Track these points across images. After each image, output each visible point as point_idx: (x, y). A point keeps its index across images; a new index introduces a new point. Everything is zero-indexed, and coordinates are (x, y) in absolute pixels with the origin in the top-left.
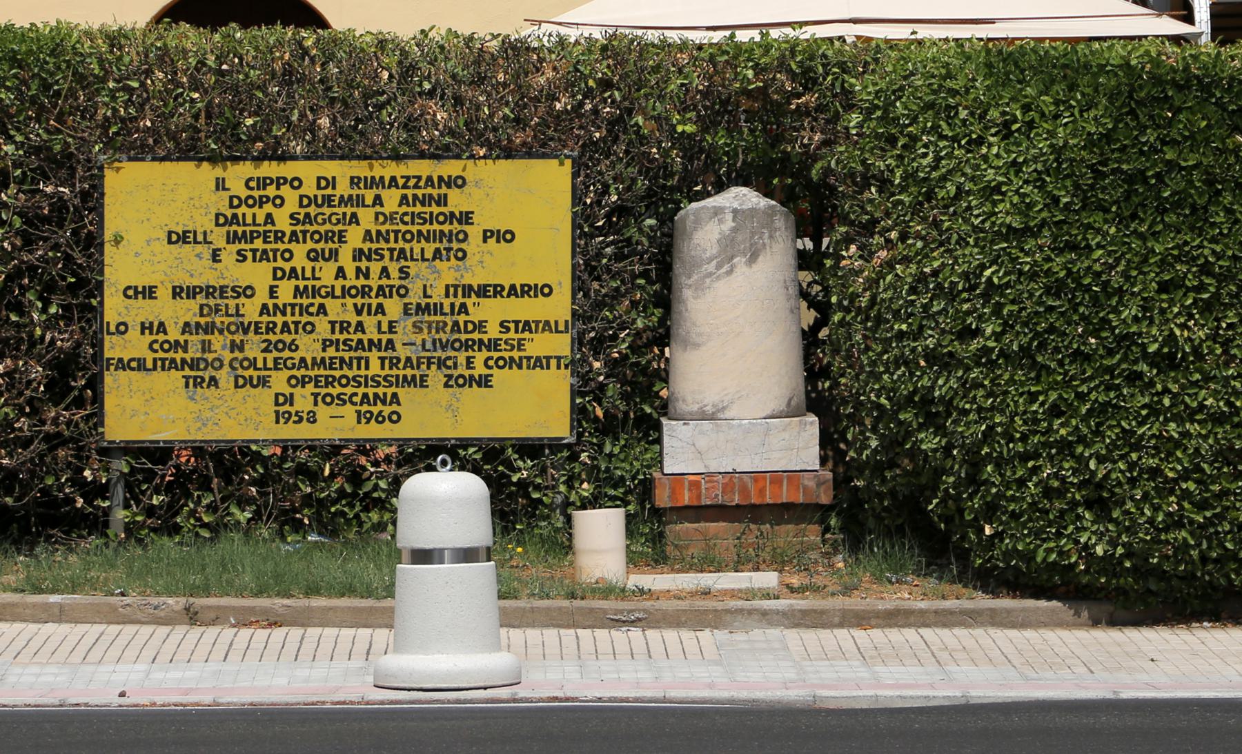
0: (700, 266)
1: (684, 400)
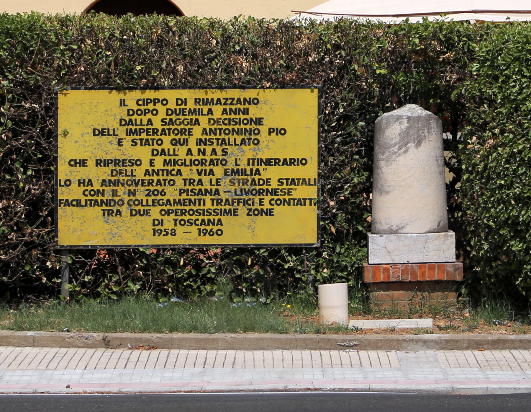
0: (389, 148)
1: (380, 223)
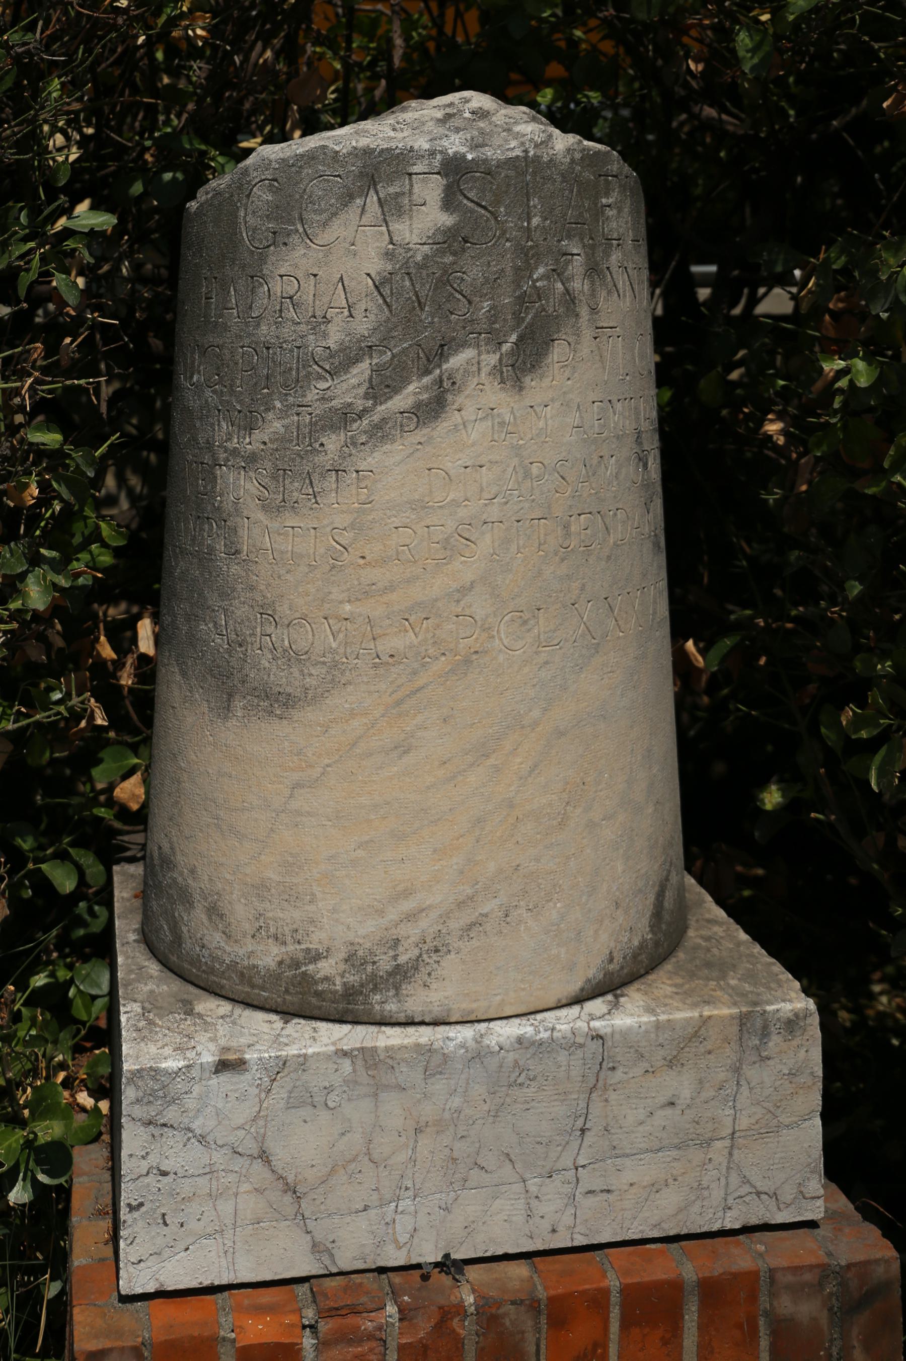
0: (301, 383)
1: (214, 912)
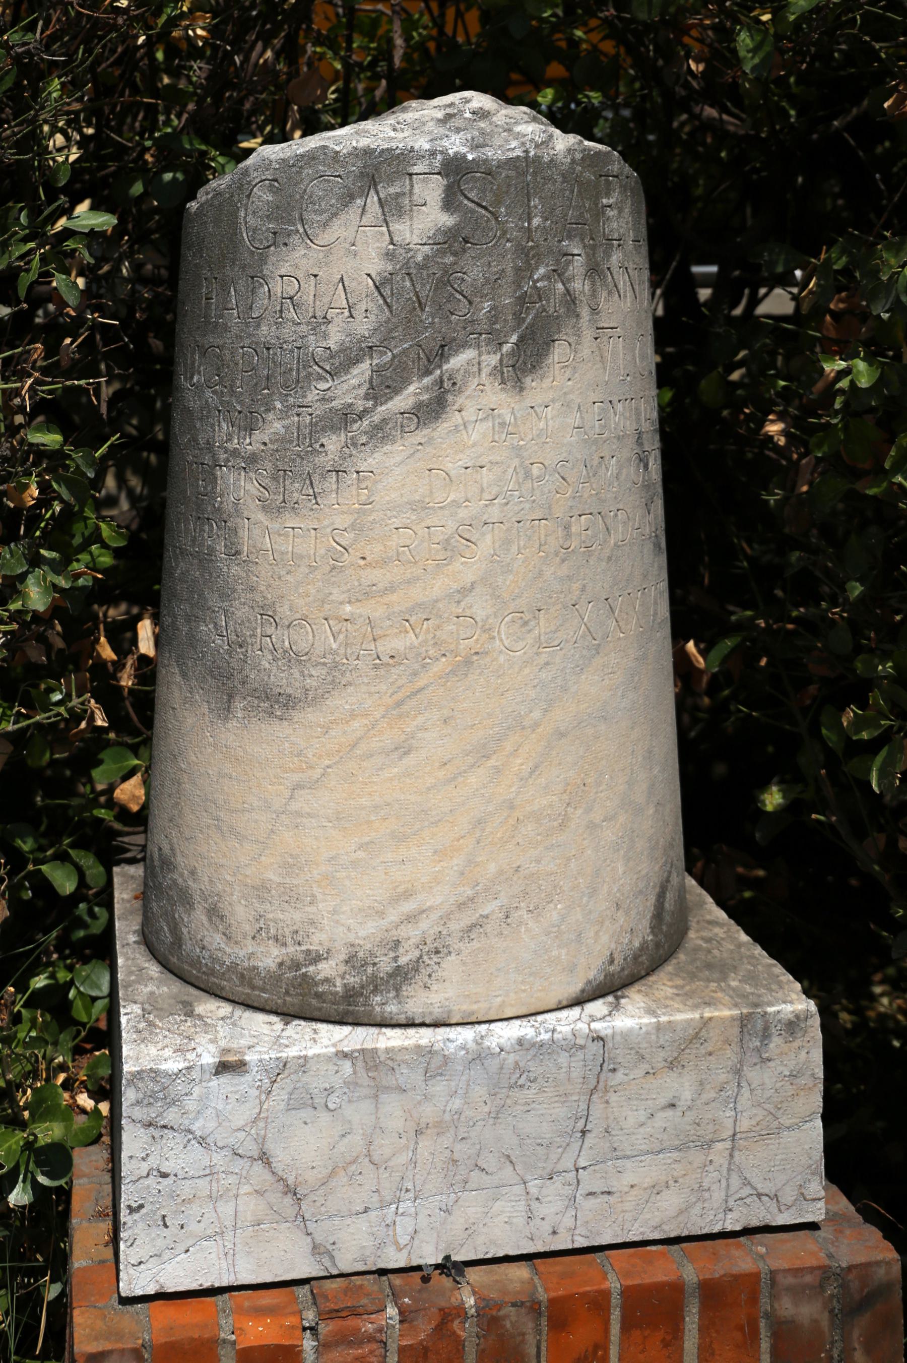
0: (301, 383)
1: (215, 913)
